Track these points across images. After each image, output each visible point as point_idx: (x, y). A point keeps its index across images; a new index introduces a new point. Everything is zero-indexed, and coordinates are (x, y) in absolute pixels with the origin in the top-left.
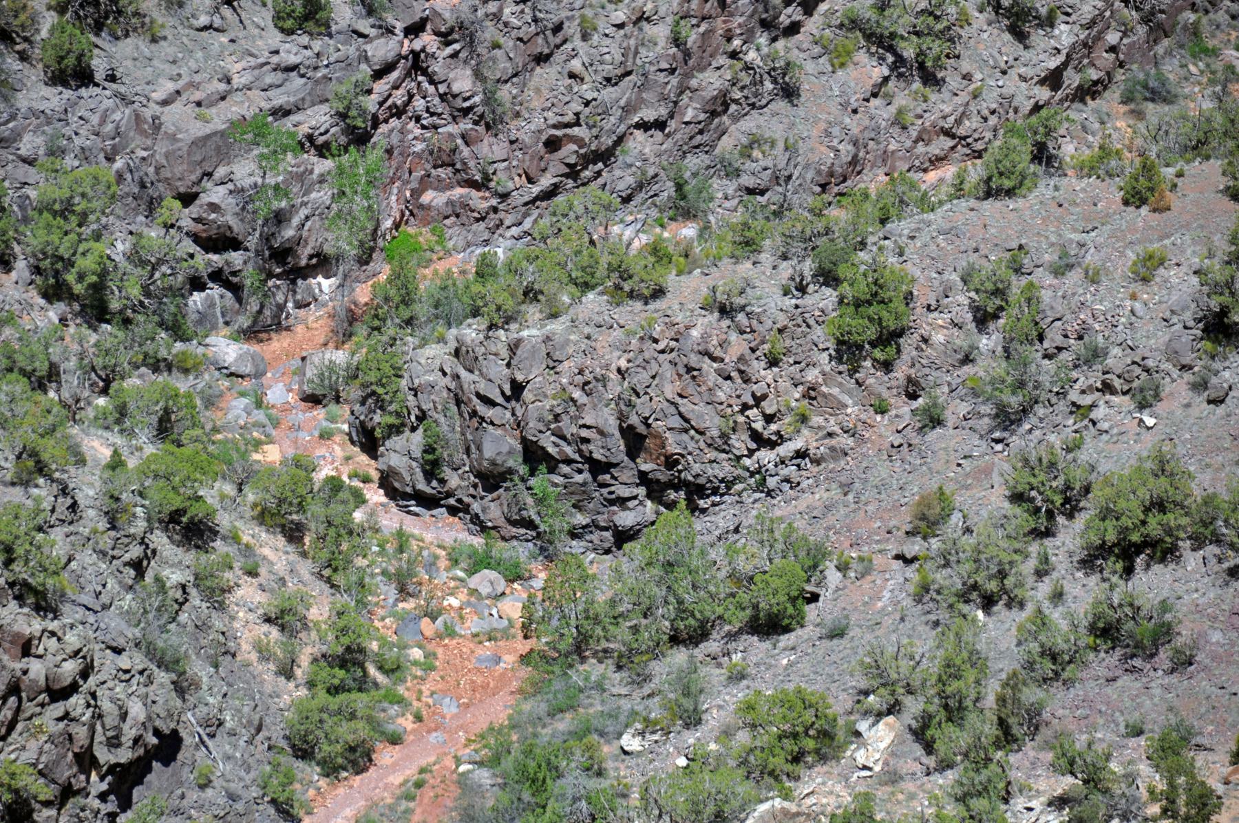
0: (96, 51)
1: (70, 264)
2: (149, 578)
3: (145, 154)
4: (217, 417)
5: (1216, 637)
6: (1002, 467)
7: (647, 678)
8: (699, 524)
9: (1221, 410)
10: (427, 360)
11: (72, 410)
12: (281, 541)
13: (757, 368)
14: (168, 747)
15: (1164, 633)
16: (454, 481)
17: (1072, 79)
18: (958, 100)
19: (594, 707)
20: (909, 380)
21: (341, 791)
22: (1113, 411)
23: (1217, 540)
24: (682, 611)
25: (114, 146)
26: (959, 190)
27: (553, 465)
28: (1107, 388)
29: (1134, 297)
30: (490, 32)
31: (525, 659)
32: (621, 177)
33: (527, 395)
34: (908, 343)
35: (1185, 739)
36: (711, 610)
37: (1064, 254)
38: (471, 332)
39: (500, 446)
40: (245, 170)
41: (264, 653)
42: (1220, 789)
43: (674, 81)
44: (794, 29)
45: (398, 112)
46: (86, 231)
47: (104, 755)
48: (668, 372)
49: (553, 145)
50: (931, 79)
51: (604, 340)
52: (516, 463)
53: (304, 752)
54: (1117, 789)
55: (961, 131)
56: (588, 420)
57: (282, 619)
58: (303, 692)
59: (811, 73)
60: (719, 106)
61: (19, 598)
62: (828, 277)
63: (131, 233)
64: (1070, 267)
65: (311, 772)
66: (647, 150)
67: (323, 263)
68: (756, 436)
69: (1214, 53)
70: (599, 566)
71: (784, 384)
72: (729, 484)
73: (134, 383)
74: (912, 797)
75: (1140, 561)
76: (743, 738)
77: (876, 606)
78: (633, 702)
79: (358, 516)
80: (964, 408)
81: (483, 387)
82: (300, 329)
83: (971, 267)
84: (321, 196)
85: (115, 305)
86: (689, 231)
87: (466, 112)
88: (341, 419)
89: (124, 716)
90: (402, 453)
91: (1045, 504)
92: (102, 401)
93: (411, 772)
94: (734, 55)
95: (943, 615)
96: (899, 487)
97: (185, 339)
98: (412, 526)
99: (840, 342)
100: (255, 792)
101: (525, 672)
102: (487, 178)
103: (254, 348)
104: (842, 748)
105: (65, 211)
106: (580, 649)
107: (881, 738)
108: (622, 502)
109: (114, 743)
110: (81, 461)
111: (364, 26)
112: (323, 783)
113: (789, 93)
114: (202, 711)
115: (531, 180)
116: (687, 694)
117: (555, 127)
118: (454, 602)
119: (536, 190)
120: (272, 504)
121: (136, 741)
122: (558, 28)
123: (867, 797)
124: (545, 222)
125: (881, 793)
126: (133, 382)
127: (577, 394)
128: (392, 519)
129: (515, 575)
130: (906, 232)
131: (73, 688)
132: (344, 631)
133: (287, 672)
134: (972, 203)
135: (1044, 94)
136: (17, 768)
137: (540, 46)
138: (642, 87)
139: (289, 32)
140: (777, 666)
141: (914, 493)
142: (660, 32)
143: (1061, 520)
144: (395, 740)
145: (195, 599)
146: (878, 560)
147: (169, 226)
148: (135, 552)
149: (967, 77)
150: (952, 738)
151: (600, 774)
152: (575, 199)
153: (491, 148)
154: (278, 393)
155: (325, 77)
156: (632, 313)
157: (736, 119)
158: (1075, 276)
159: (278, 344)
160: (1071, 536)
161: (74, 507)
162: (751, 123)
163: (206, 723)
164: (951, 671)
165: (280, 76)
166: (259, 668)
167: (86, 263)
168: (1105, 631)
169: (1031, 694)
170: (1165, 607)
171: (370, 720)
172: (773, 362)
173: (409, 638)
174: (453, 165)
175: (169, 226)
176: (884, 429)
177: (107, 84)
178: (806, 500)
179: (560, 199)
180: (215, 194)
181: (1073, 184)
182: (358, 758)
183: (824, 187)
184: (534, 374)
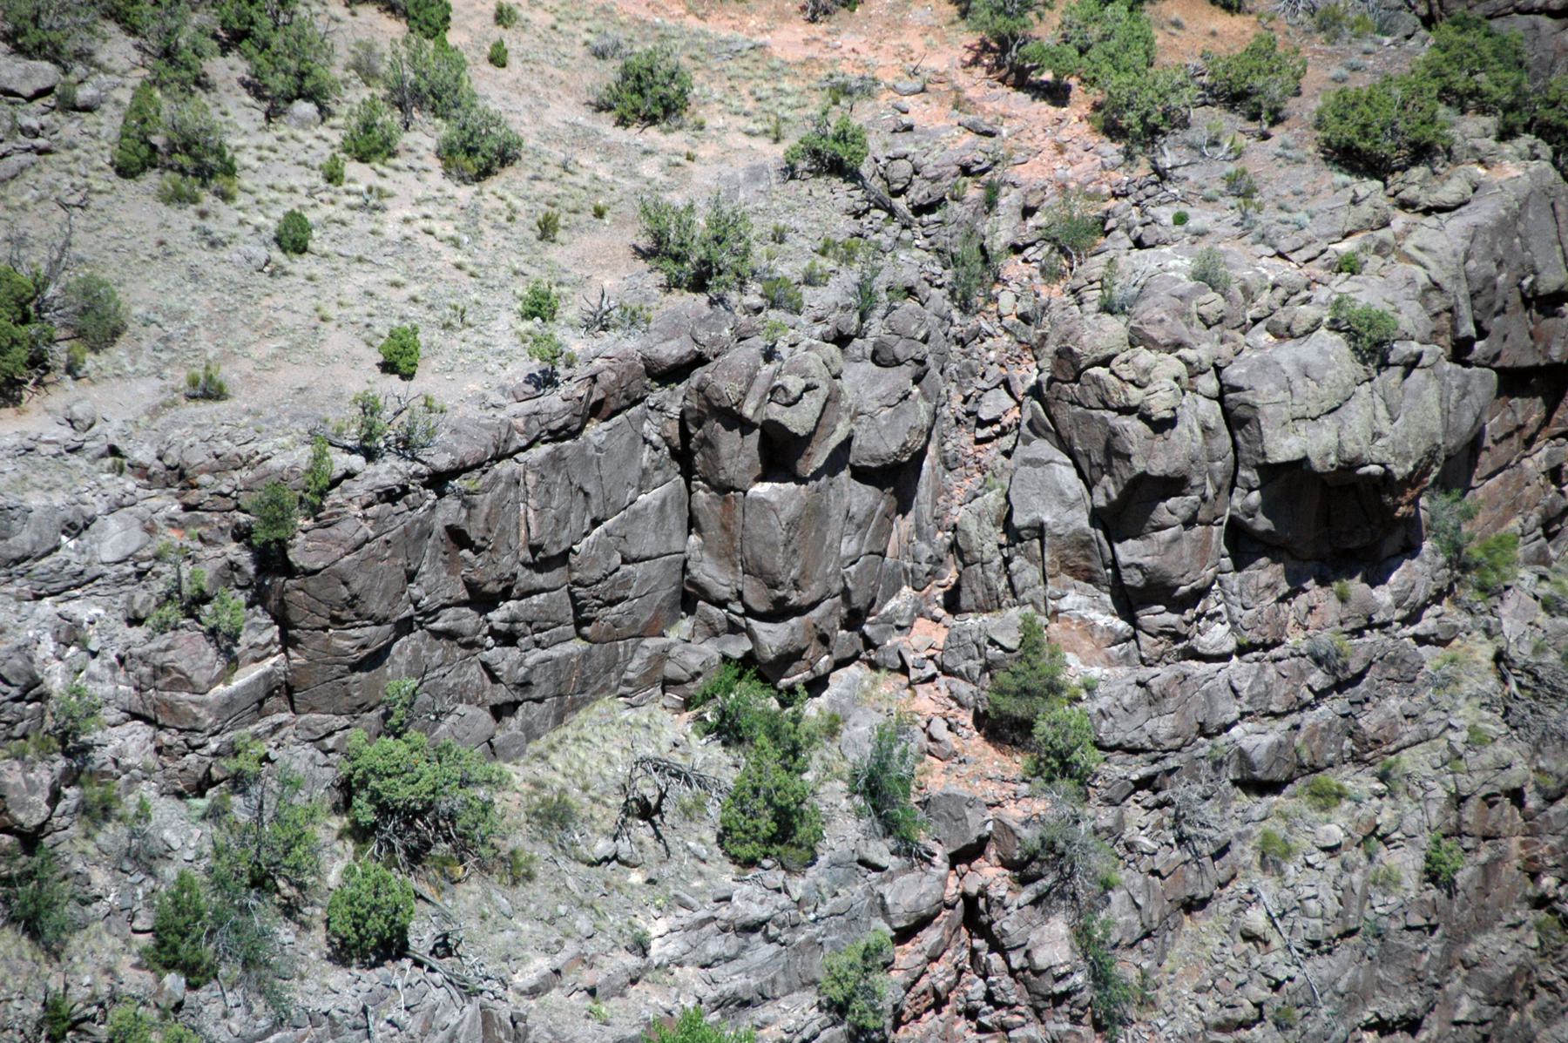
142: (1406, 862)
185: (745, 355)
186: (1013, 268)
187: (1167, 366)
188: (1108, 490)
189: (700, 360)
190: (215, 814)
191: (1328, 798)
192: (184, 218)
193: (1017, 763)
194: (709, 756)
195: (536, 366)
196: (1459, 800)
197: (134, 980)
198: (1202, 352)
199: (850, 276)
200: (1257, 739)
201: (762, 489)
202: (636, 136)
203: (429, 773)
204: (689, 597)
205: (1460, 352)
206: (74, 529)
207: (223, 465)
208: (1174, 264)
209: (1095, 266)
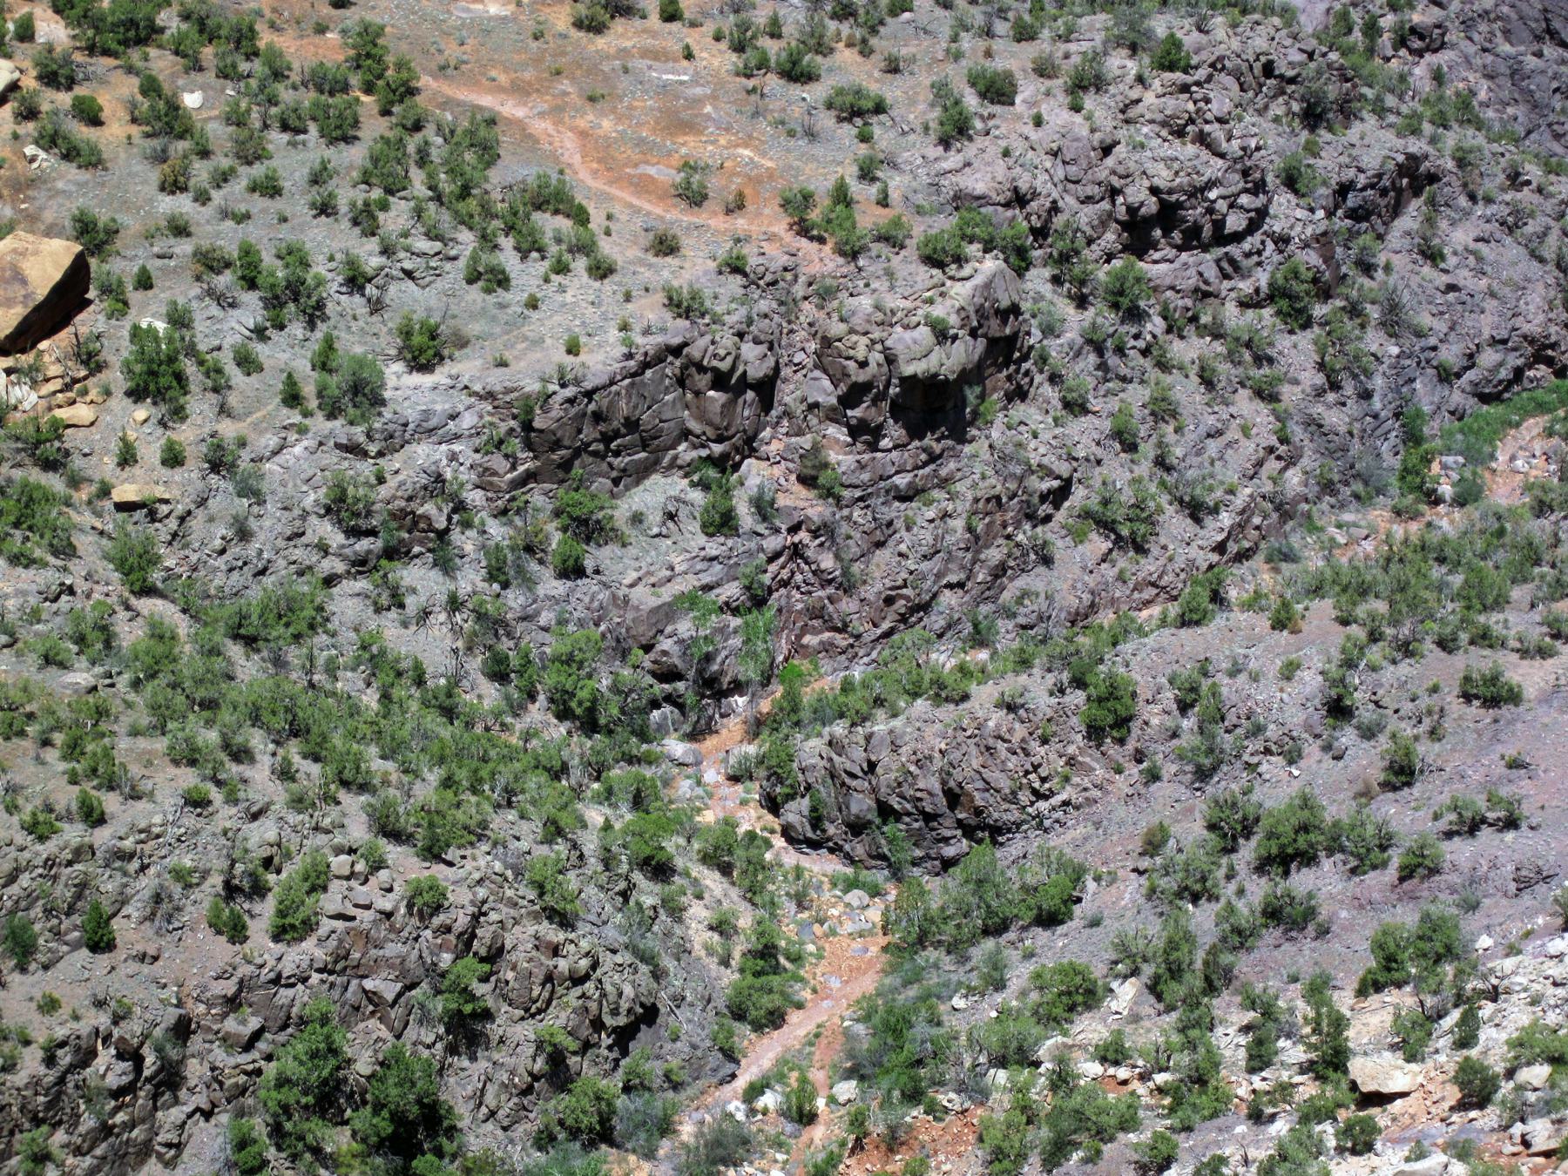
1: (573, 695)
2: (632, 903)
4: (672, 793)
5: (1344, 914)
6: (1201, 807)
7: (968, 959)
8: (999, 854)
9: (1341, 764)
10: (810, 749)
11: (578, 792)
12: (717, 875)
13: (1034, 746)
14: (649, 1014)
15: (1310, 913)
16: (831, 830)
17: (1233, 548)
19: (933, 979)
20: (1137, 750)
21: (765, 1041)
22: (1272, 767)
23: (1342, 850)
24: (990, 912)
26: (1163, 622)
27: (898, 816)
28: (1267, 751)
30: (844, 528)
31: (885, 949)
32: (936, 621)
33: (879, 770)
34: (1135, 726)
35: (1326, 983)
36: (1009, 911)
37: (1235, 663)
38: (839, 729)
39: (861, 804)
40: (685, 627)
41: (710, 951)
42: (1348, 1014)
43: (969, 556)
44: (1047, 519)
45: (785, 584)
46: (583, 673)
47: (609, 1021)
48: (974, 750)
49: (889, 601)
50: (1141, 549)
51: (929, 731)
52: (873, 816)
53: (739, 1014)
54: (1283, 1018)
56: (921, 785)
57: (722, 927)
58: (737, 976)
59: (1060, 547)
60: (1000, 571)
61: (549, 918)
62: (1079, 683)
65: (744, 1029)
67: (738, 687)
68: (1035, 792)
69: (1322, 530)
70: (932, 884)
71: (1053, 756)
72: (1018, 826)
73: (617, 772)
74: (1149, 1031)
75: (1293, 866)
76: (1035, 996)
77: (1120, 904)
78: (960, 975)
79: (768, 856)
80: (1174, 768)
81: (848, 766)
82: (724, 732)
85: (602, 721)
86: (983, 655)
87: (830, 582)
88: (754, 791)
89: (620, 995)
90: (797, 811)
91: (1230, 830)
92: (596, 786)
93: (810, 1027)
94: (1008, 537)
95: (1166, 908)
96: (1130, 823)
97: (649, 742)
98: (805, 862)
99: (1089, 727)
100: (708, 1043)
101: (886, 957)
102: (846, 625)
103: (695, 746)
104: (1100, 1000)
105: (568, 660)
106: (922, 941)
107: (1126, 994)
108: (946, 840)
109: (615, 1012)
110: (585, 826)
111: (761, 528)
112: (753, 1036)
113: (1047, 561)
114: (671, 990)
116: (995, 968)
118: (834, 912)
119: (879, 631)
120: (711, 851)
121: (629, 1011)
122: (890, 524)
123: (1119, 1032)
124: (886, 653)
125: (1128, 1029)
126: (616, 772)
127: (913, 768)
128: (791, 858)
129: (875, 892)
131: (586, 978)
132: (762, 934)
133: (725, 962)
135: (1215, 558)
136: (555, 1029)
137: (878, 536)
138: (948, 561)
139: (711, 535)
140: (1058, 948)
141: (1143, 827)
142: (958, 524)
143: (1241, 841)
144: (800, 1006)
145: (663, 916)
146: (1121, 873)
147: (636, 667)
148: (622, 885)
149: (1164, 548)
150: (1175, 990)
151: (939, 1024)
152: (907, 637)
153: (848, 605)
154: (712, 775)
156: (948, 712)
157: (1011, 579)
158: (1242, 678)
159: (710, 742)
160: (1248, 851)
161: (581, 857)
162: (1022, 582)
163: (674, 998)
164: (1172, 946)
166: (706, 960)
167: (583, 694)
168: (1273, 914)
169: (1226, 958)
170: (1310, 896)
171: (782, 993)
172: (1045, 741)
173: (806, 938)
175: (636, 667)
176: (1121, 784)
178: (1070, 835)
179: (896, 637)
180: (666, 644)
181: (1240, 617)
182: (776, 1019)
183: (1073, 623)
184: (884, 756)
185: (703, 342)
186: (806, 306)
187: (864, 340)
188: (843, 388)
189: (686, 344)
190: (510, 523)
191: (928, 503)
192: (491, 299)
193: (812, 494)
194: (697, 496)
195: (625, 350)
196: (977, 500)
197: (482, 586)
198: (876, 335)
199: (743, 311)
200: (901, 481)
201: (711, 393)
202: (659, 260)
203: (591, 505)
204: (686, 434)
205: (973, 333)
206: (453, 417)
207: (508, 391)
208: (865, 302)
209: (835, 304)
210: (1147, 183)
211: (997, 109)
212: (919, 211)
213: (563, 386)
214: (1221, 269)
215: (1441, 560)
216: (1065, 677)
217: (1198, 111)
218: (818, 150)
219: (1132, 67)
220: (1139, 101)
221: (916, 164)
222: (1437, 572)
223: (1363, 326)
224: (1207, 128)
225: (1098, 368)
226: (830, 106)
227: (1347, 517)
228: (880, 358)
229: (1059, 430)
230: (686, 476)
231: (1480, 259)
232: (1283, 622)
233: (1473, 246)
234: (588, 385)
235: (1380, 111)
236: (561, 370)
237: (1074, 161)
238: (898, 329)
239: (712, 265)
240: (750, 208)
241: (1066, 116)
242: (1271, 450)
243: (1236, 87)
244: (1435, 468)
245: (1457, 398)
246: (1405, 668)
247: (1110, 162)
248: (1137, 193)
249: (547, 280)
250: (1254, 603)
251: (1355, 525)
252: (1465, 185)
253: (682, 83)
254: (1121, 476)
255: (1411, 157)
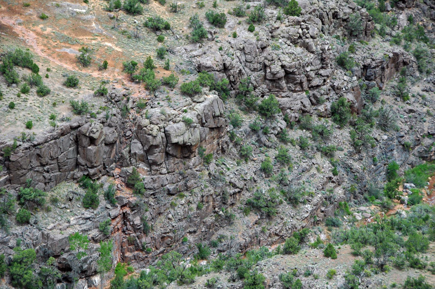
0: (32, 216)
3: (45, 244)
18: (280, 225)
25: (36, 243)
29: (327, 283)
55: (281, 234)
62: (241, 277)
63: (40, 267)
64: (309, 274)
66: (191, 240)
83: (282, 275)
84: (96, 255)
86: (204, 263)
115: (157, 249)
117: (164, 233)
119: (158, 252)
130: (263, 264)
134: (282, 256)
149: (282, 219)
155: (97, 221)
158: (310, 277)
162: (221, 232)
165: (85, 221)
174: (134, 245)
177: (34, 225)
185: (86, 126)
186: (132, 111)
187: (156, 127)
188: (146, 148)
189: (79, 126)
194: (81, 191)
198: (161, 125)
199: (105, 113)
201: (90, 147)
205: (203, 125)
209: (144, 111)
210: (280, 64)
211: (217, 30)
212: (183, 72)
213: (24, 142)
214: (311, 101)
215: (400, 229)
216: (235, 274)
217: (303, 34)
218: (140, 44)
219: (276, 12)
220: (278, 28)
221: (183, 53)
222: (397, 234)
223: (371, 126)
224: (307, 40)
225: (257, 141)
226: (146, 25)
227: (362, 208)
228: (163, 135)
229: (238, 168)
230: (78, 182)
231: (423, 97)
232: (329, 253)
233: (421, 93)
234: (36, 143)
235: (382, 33)
236: (24, 134)
237: (250, 53)
238: (171, 123)
239: (92, 92)
240: (109, 68)
241: (247, 34)
242: (330, 178)
243: (320, 23)
244: (401, 189)
245: (412, 158)
246: (380, 277)
247: (265, 54)
248: (276, 68)
249: (19, 96)
250: (317, 244)
251: (365, 211)
252: (419, 67)
253: (81, 13)
254: (264, 187)
255: (396, 55)
